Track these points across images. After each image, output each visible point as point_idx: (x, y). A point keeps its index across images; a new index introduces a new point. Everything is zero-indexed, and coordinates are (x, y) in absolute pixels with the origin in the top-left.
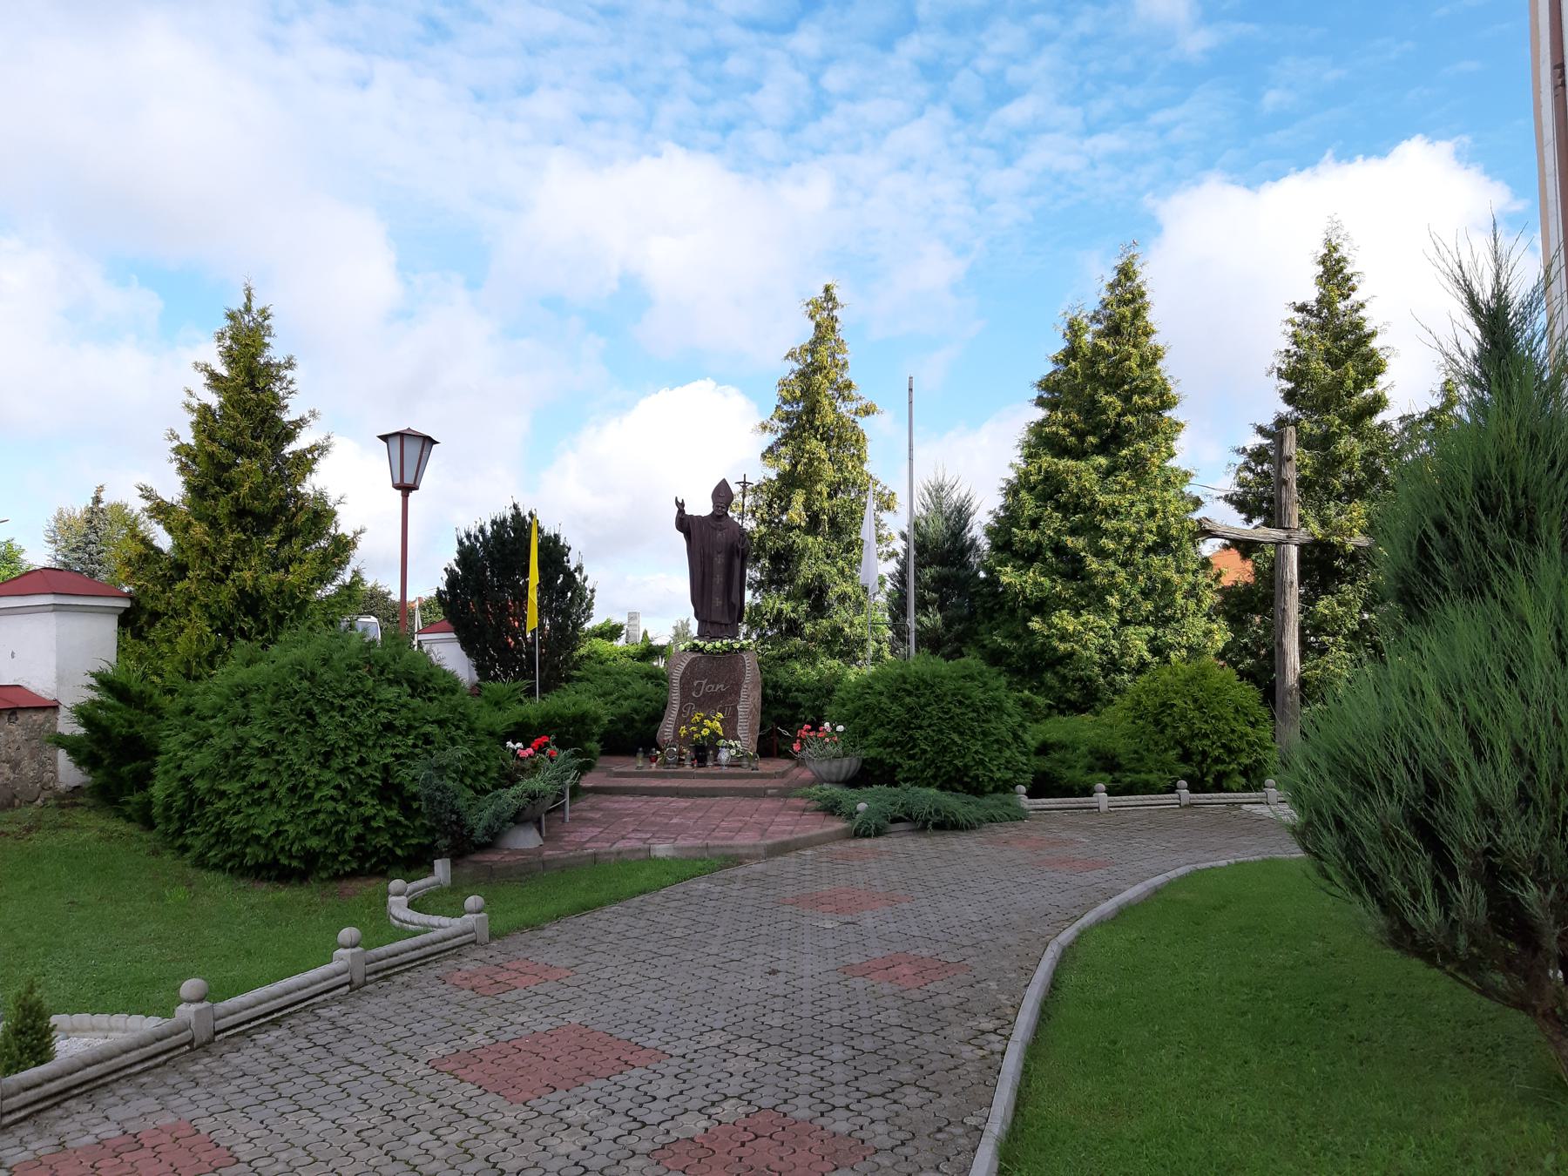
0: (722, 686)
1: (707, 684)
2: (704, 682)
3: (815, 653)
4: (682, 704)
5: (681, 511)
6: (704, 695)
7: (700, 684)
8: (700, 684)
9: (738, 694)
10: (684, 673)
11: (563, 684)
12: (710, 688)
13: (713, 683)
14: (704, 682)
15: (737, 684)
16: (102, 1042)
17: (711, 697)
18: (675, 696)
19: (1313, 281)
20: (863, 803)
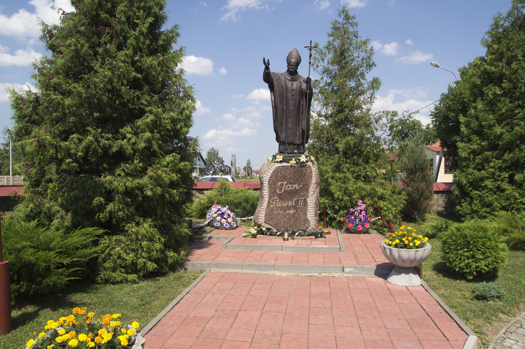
0: (297, 185)
1: (286, 185)
2: (285, 183)
3: (346, 118)
4: (270, 197)
5: (267, 68)
6: (285, 192)
7: (282, 185)
8: (282, 185)
9: (307, 190)
10: (271, 177)
11: (164, 28)
12: (289, 187)
13: (291, 183)
14: (285, 183)
15: (306, 184)
16: (449, 221)
17: (290, 193)
18: (266, 192)
19: (381, 87)
20: (96, 255)
